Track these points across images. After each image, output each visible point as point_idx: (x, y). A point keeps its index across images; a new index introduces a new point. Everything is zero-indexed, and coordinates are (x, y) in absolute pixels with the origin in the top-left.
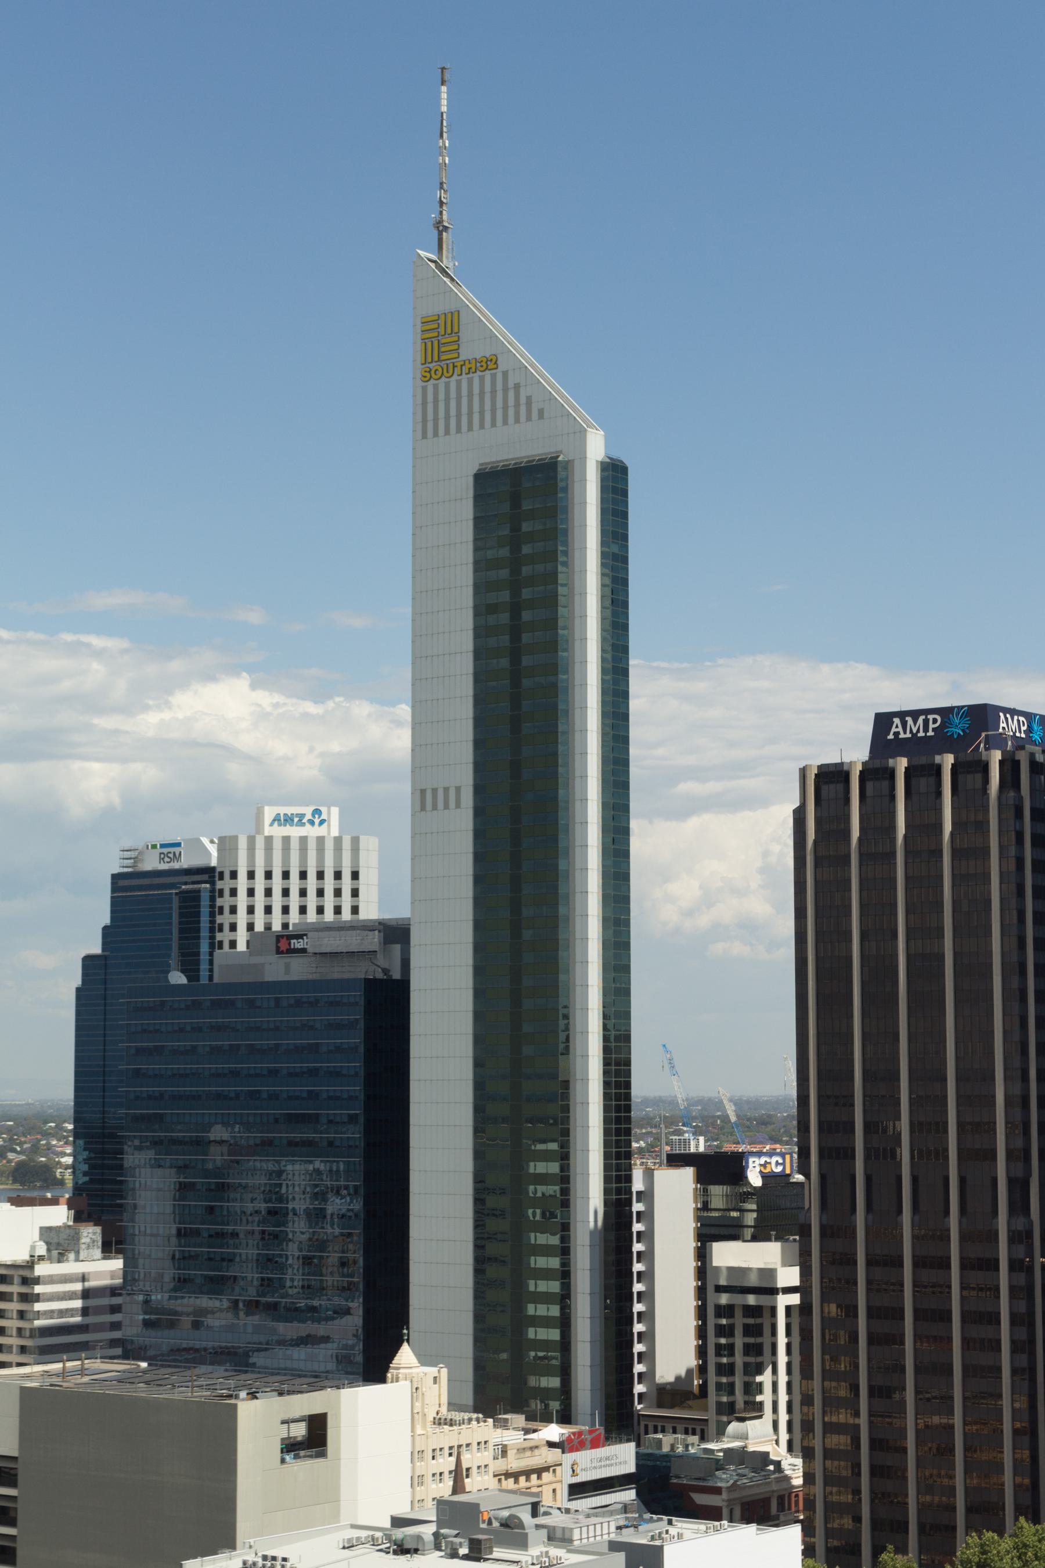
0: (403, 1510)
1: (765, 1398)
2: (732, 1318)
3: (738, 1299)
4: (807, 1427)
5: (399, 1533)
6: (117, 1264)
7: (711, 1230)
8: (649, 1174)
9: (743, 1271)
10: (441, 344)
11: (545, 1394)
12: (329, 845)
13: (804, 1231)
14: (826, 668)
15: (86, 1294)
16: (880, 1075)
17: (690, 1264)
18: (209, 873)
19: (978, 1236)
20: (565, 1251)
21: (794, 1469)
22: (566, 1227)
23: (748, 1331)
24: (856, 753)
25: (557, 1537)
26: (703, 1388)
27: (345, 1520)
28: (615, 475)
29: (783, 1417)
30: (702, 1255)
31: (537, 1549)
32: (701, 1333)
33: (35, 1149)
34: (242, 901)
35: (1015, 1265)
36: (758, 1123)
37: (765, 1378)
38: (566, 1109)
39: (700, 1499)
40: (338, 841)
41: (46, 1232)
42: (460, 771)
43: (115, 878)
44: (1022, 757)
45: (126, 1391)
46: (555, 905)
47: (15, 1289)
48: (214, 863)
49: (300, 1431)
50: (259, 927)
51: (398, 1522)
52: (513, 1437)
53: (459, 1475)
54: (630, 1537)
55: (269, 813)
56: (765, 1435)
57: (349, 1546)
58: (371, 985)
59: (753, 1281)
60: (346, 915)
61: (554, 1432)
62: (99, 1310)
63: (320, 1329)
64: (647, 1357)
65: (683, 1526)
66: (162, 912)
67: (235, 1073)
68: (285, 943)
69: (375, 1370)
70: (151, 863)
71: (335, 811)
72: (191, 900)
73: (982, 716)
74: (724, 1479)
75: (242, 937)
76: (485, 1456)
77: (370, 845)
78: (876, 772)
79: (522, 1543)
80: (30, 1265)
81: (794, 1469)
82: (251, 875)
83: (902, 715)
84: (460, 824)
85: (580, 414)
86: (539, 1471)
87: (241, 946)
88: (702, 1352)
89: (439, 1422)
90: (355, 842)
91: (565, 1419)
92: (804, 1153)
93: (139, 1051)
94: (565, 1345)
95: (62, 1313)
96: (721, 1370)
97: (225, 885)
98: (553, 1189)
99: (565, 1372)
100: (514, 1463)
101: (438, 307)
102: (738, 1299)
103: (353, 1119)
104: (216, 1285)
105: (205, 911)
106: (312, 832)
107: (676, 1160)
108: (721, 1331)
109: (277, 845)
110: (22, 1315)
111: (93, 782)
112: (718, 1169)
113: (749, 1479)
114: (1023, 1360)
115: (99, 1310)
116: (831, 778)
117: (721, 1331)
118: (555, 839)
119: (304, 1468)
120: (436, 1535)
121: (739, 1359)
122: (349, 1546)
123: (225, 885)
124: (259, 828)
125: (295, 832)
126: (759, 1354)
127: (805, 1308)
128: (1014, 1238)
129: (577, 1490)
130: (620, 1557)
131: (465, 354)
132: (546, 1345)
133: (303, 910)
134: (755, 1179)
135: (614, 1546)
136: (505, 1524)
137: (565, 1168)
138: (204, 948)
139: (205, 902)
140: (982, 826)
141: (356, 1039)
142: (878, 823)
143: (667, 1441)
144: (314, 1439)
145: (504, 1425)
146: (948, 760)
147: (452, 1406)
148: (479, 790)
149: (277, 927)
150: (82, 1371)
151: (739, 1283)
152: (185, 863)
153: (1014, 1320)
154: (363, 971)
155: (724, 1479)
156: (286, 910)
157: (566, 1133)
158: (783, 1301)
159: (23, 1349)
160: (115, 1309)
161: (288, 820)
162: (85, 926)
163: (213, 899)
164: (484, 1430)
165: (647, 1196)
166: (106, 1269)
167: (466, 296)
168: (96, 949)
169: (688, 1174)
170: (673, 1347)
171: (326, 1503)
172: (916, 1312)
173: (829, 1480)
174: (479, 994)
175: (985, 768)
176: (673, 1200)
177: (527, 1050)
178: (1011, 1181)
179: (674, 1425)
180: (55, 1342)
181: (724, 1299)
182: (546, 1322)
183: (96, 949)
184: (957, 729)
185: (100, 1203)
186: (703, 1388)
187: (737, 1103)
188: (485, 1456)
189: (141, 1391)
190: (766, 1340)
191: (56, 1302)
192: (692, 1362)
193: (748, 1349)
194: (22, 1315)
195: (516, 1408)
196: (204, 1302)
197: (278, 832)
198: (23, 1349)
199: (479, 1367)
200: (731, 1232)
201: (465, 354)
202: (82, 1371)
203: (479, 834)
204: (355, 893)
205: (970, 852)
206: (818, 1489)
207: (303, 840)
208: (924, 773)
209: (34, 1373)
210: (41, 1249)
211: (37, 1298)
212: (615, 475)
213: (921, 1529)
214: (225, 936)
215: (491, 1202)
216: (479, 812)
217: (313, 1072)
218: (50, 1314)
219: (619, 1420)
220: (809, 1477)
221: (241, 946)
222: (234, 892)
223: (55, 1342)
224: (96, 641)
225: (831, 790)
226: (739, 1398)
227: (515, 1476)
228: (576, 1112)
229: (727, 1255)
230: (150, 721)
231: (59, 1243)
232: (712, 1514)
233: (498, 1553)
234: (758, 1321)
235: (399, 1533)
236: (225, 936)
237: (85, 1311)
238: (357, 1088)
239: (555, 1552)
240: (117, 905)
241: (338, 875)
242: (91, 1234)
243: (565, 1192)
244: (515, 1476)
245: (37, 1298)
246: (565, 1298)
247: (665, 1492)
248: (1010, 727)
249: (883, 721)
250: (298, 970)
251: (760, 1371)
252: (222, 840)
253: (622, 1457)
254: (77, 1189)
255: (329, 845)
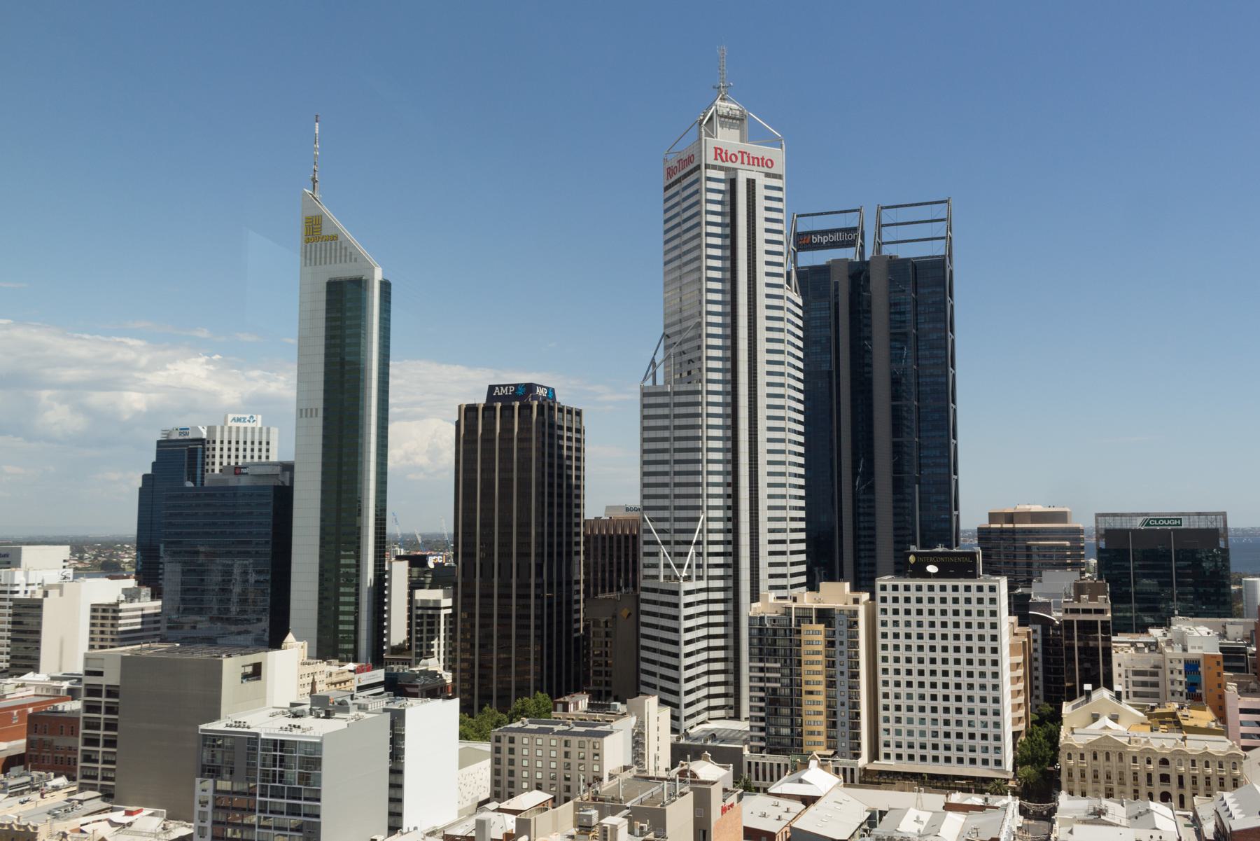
0: (294, 700)
1: (435, 650)
2: (422, 620)
3: (425, 612)
4: (454, 660)
5: (294, 709)
6: (159, 603)
7: (414, 585)
8: (390, 563)
9: (428, 601)
10: (314, 229)
11: (347, 651)
12: (257, 431)
13: (455, 585)
14: (444, 367)
15: (143, 616)
16: (487, 524)
17: (406, 598)
18: (202, 441)
19: (523, 586)
20: (357, 594)
21: (448, 677)
22: (357, 585)
23: (429, 624)
24: (481, 400)
25: (362, 708)
26: (410, 647)
27: (269, 704)
28: (386, 286)
29: (442, 657)
30: (411, 595)
31: (353, 713)
32: (410, 625)
33: (111, 555)
34: (218, 453)
35: (537, 597)
36: (433, 544)
37: (435, 642)
38: (359, 538)
39: (409, 690)
40: (261, 429)
41: (125, 591)
42: (317, 401)
43: (159, 442)
44: (546, 404)
45: (170, 656)
46: (357, 457)
47: (110, 614)
48: (205, 436)
49: (249, 670)
50: (225, 464)
51: (293, 705)
52: (334, 668)
53: (313, 684)
54: (391, 706)
55: (230, 417)
56: (435, 664)
57: (273, 715)
58: (276, 488)
59: (431, 605)
60: (264, 459)
61: (351, 666)
62: (149, 623)
63: (250, 628)
64: (389, 635)
65: (411, 701)
66: (179, 459)
67: (214, 524)
68: (237, 470)
69: (276, 642)
70: (175, 436)
71: (260, 417)
72: (193, 453)
73: (530, 387)
74: (420, 682)
75: (217, 468)
76: (323, 677)
77: (275, 433)
78: (489, 408)
79: (347, 710)
80: (117, 604)
81: (448, 677)
82: (222, 442)
83: (499, 386)
84: (318, 422)
85: (373, 261)
86: (345, 682)
87: (217, 471)
88: (409, 633)
89: (303, 664)
90: (268, 429)
91: (355, 661)
92: (456, 555)
93: (171, 514)
94: (356, 632)
95: (132, 624)
96: (417, 640)
97: (211, 446)
98: (353, 570)
99: (356, 642)
100: (334, 679)
101: (313, 213)
102: (425, 612)
103: (267, 542)
104: (200, 611)
105: (199, 456)
106: (249, 425)
107: (399, 558)
108: (418, 624)
109: (234, 430)
110: (113, 625)
111: (134, 400)
112: (417, 562)
113: (429, 681)
114: (539, 632)
115: (149, 623)
116: (470, 410)
117: (418, 624)
118: (357, 431)
119: (251, 685)
120: (311, 710)
121: (425, 636)
122: (273, 715)
123: (211, 446)
124: (226, 422)
125: (242, 425)
126: (433, 633)
127: (453, 615)
128: (537, 586)
129: (360, 689)
130: (388, 715)
131: (324, 233)
132: (347, 632)
133: (245, 457)
134: (431, 565)
135: (385, 710)
136: (340, 704)
137: (358, 561)
138: (199, 472)
139: (200, 453)
140: (529, 430)
141: (270, 510)
142: (489, 427)
143: (395, 668)
144: (256, 672)
145: (329, 664)
146: (517, 404)
147: (309, 657)
148: (325, 409)
149: (233, 463)
150: (149, 648)
151: (425, 605)
152: (191, 436)
153: (536, 617)
154: (272, 482)
155: (420, 682)
156: (237, 457)
157: (359, 547)
158: (443, 612)
159: (113, 640)
160: (156, 622)
161: (239, 420)
162: (146, 461)
163: (203, 452)
164: (322, 666)
165: (390, 572)
166: (152, 606)
167: (325, 210)
168: (149, 471)
169: (406, 563)
170: (398, 632)
171: (261, 698)
172: (499, 615)
173: (462, 680)
174: (323, 492)
175: (531, 407)
176: (400, 573)
177: (343, 515)
178: (537, 565)
179: (398, 662)
180: (129, 637)
181: (420, 612)
182: (348, 623)
183: (149, 471)
184: (520, 393)
185: (149, 576)
186: (410, 647)
187: (423, 536)
188: (323, 677)
189: (177, 656)
190: (436, 627)
191: (130, 619)
192: (405, 637)
193: (428, 631)
194: (113, 625)
195: (335, 657)
196: (198, 618)
197: (234, 425)
198: (113, 640)
199: (319, 641)
200: (421, 586)
201: (324, 233)
202: (149, 648)
203: (325, 428)
204: (268, 450)
205: (524, 439)
206: (458, 684)
207: (245, 428)
208: (507, 409)
209: (126, 650)
210: (123, 597)
211: (120, 618)
212: (386, 286)
213: (498, 697)
214: (210, 467)
215: (327, 575)
216: (325, 419)
217: (250, 523)
218: (126, 625)
219: (377, 660)
220: (454, 679)
221: (217, 471)
222: (214, 449)
223: (129, 637)
224: (131, 342)
225: (471, 414)
226: (424, 651)
227: (335, 684)
228: (363, 540)
229: (421, 595)
230: (158, 378)
231: (131, 595)
232: (415, 695)
233: (337, 715)
234: (433, 620)
235: (294, 709)
236: (210, 467)
237: (142, 623)
238: (270, 530)
239: (361, 714)
240: (159, 453)
241: (260, 443)
242: (146, 591)
243: (358, 571)
244: (335, 684)
245: (120, 618)
246: (356, 613)
247: (397, 687)
248: (541, 392)
249: (492, 388)
250: (244, 481)
251: (433, 639)
252: (209, 428)
253: (379, 675)
254: (137, 573)
255: (257, 431)
